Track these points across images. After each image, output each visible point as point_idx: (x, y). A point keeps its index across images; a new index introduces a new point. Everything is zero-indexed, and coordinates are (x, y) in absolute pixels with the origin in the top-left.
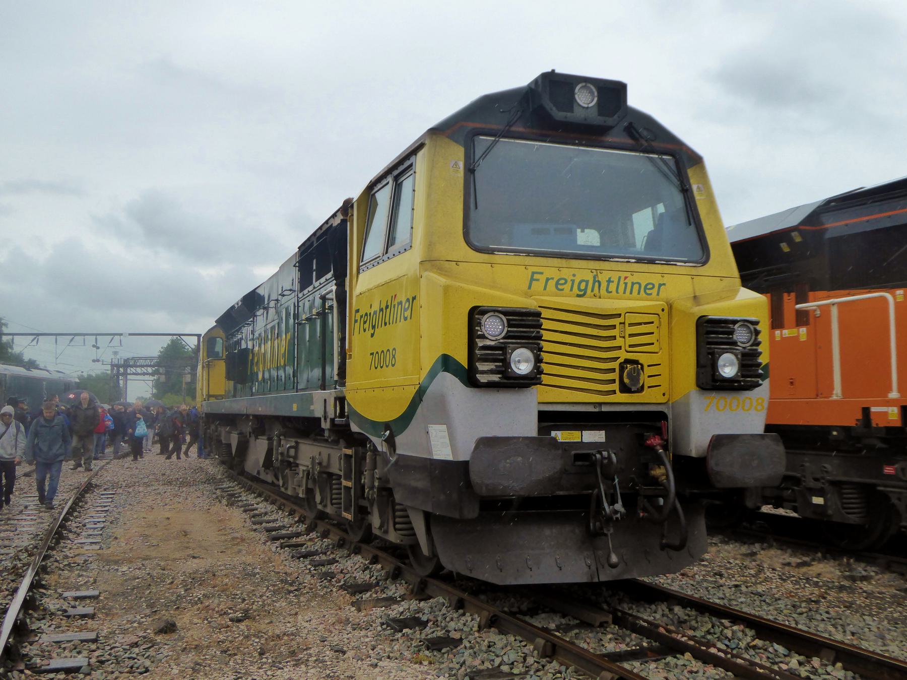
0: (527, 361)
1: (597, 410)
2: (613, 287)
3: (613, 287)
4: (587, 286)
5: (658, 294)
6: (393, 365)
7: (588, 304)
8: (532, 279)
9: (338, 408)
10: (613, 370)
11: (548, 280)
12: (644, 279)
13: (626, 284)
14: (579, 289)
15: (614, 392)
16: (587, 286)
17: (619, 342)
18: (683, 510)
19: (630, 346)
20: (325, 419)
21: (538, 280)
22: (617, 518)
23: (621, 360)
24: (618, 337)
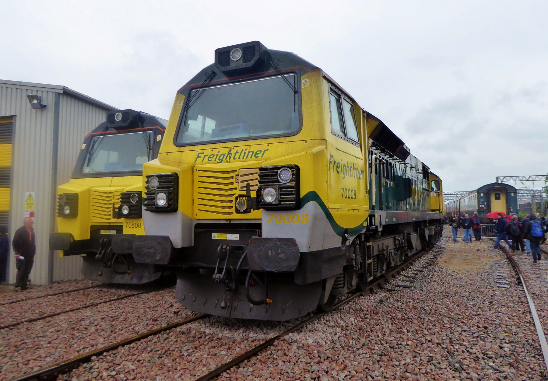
0: (164, 199)
1: (228, 222)
2: (237, 155)
3: (237, 155)
4: (223, 157)
5: (262, 156)
7: (224, 166)
8: (198, 157)
9: (373, 221)
10: (232, 201)
11: (205, 156)
12: (255, 149)
13: (245, 153)
14: (219, 159)
15: (232, 213)
16: (223, 157)
17: (235, 185)
18: (245, 280)
20: (380, 226)
23: (237, 195)
24: (234, 183)
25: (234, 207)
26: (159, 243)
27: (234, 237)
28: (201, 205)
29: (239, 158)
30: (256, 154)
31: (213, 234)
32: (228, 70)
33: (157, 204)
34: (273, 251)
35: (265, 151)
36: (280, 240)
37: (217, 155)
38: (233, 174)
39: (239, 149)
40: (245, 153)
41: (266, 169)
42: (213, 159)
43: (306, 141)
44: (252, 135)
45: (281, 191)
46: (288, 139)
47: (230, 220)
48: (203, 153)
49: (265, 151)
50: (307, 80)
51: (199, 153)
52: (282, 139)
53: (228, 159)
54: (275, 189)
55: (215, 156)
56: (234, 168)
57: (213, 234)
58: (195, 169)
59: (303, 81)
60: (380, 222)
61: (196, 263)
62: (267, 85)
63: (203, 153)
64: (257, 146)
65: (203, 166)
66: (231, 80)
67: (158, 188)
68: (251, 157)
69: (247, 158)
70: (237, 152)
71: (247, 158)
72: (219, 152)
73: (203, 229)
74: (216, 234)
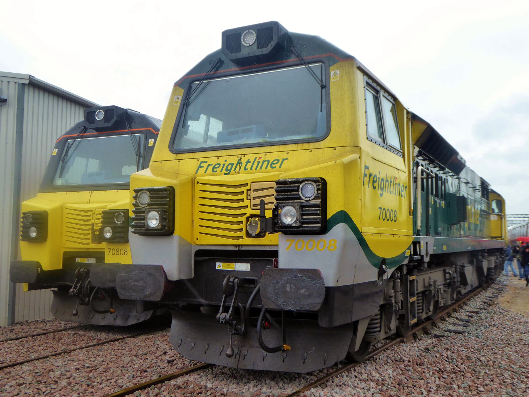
1: (237, 249)
2: (249, 166)
3: (249, 166)
5: (280, 167)
6: (395, 221)
7: (233, 178)
8: (200, 166)
10: (242, 222)
11: (209, 165)
12: (271, 157)
13: (259, 162)
14: (227, 170)
15: (242, 237)
17: (246, 203)
19: (254, 205)
20: (427, 255)
21: (203, 167)
22: (222, 322)
23: (248, 215)
24: (245, 199)
27: (244, 267)
29: (251, 169)
30: (272, 163)
31: (218, 264)
33: (148, 225)
36: (301, 271)
38: (244, 189)
39: (252, 158)
40: (259, 162)
41: (284, 183)
43: (335, 148)
45: (303, 211)
46: (312, 145)
47: (239, 246)
48: (206, 162)
49: (284, 160)
51: (202, 162)
52: (306, 146)
53: (237, 170)
54: (295, 208)
55: (222, 166)
56: (245, 180)
57: (218, 264)
58: (196, 182)
59: (332, 73)
62: (289, 77)
63: (206, 162)
64: (274, 153)
67: (149, 205)
68: (266, 168)
69: (261, 168)
70: (249, 161)
71: (261, 168)
72: (226, 161)
74: (221, 264)
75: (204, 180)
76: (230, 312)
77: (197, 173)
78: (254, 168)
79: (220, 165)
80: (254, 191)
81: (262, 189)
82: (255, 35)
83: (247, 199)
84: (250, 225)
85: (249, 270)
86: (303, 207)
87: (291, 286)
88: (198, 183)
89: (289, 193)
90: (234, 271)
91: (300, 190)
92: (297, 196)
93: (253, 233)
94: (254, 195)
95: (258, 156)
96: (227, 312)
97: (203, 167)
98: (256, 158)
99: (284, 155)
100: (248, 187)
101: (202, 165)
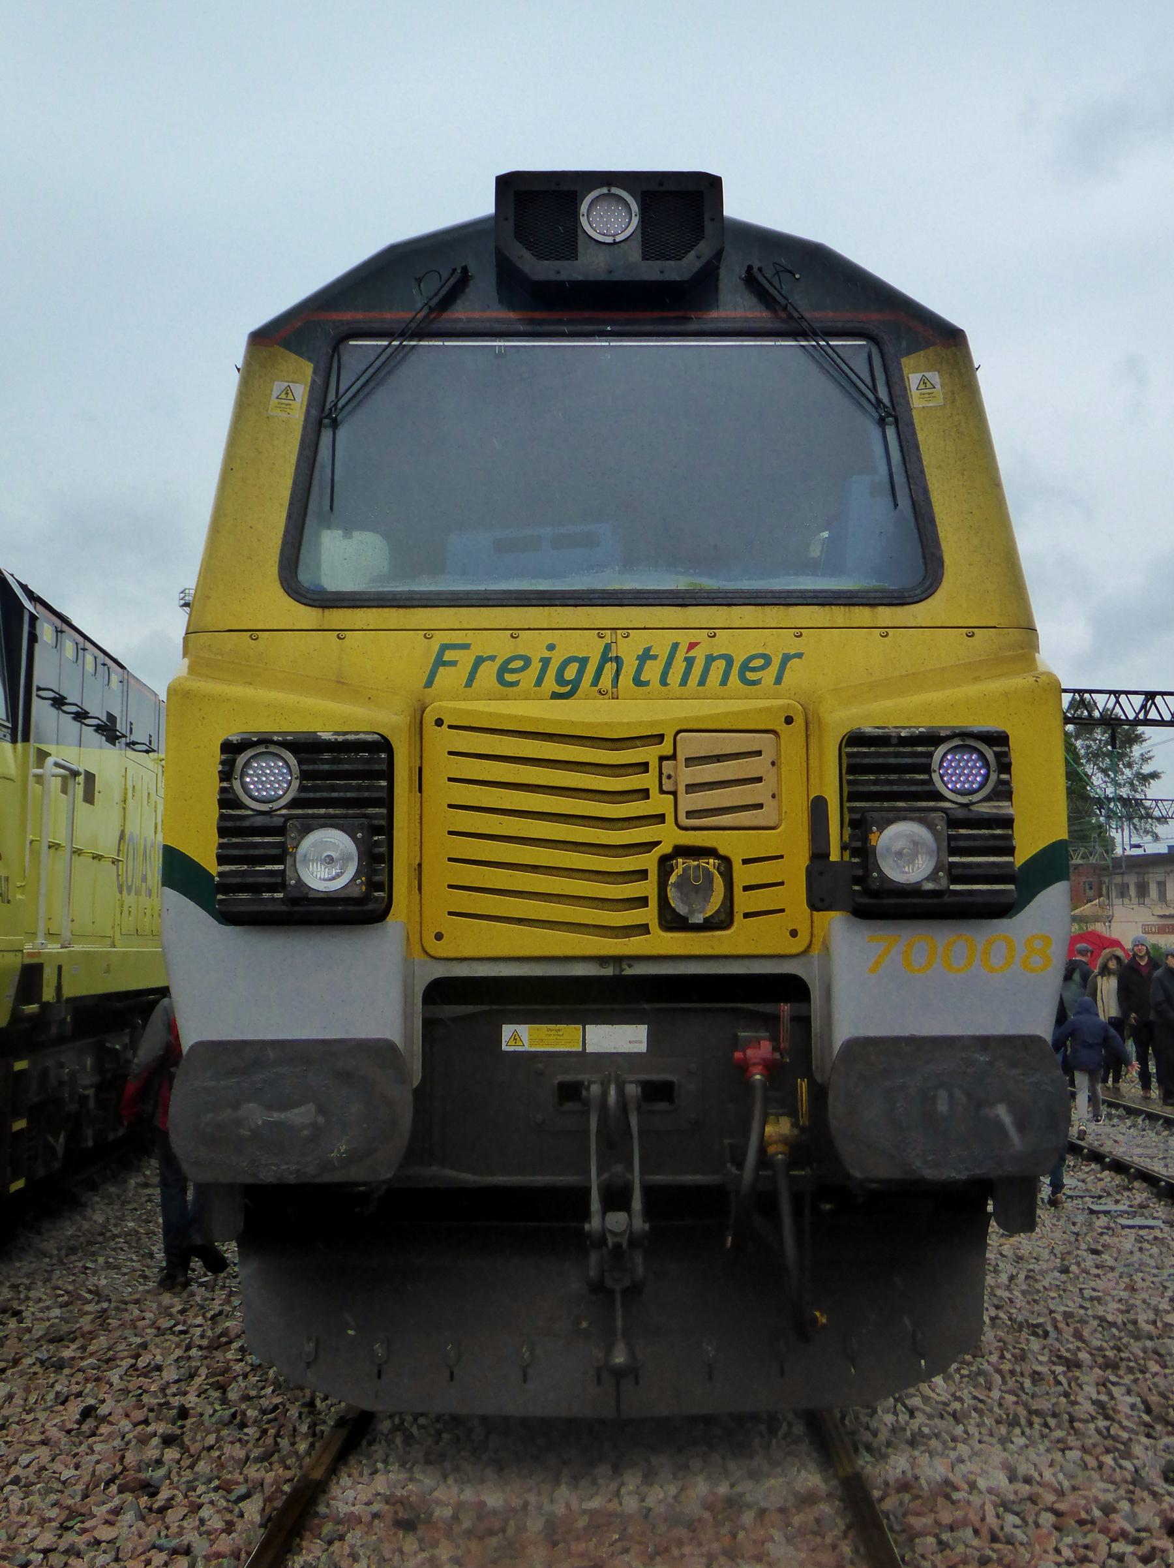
1: (609, 971)
2: (652, 672)
3: (652, 672)
4: (581, 673)
7: (586, 712)
8: (440, 662)
10: (643, 874)
11: (479, 661)
12: (741, 646)
13: (690, 662)
14: (560, 680)
15: (644, 929)
17: (659, 803)
19: (689, 814)
21: (454, 663)
23: (665, 848)
25: (653, 903)
26: (346, 1077)
27: (624, 1038)
28: (491, 895)
29: (664, 682)
30: (745, 667)
31: (507, 1030)
32: (564, 276)
33: (300, 883)
34: (958, 1093)
35: (786, 658)
36: (984, 1042)
37: (546, 662)
38: (649, 754)
39: (661, 644)
40: (690, 662)
41: (881, 740)
42: (528, 678)
43: (970, 631)
44: (709, 583)
45: (283, 845)
46: (885, 615)
47: (618, 960)
48: (466, 647)
49: (786, 658)
50: (934, 377)
51: (444, 648)
52: (862, 615)
53: (606, 681)
54: (931, 826)
55: (536, 666)
56: (653, 723)
57: (507, 1030)
58: (429, 718)
59: (913, 380)
60: (59, 988)
61: (435, 1169)
62: (728, 371)
63: (466, 647)
64: (744, 633)
65: (481, 706)
66: (531, 322)
67: (294, 803)
68: (724, 682)
69: (702, 682)
70: (646, 656)
71: (702, 682)
72: (551, 647)
73: (461, 1004)
74: (524, 1030)
75: (469, 713)
76: (637, 1204)
77: (429, 683)
78: (675, 677)
79: (527, 661)
80: (690, 761)
81: (719, 758)
82: (635, 207)
83: (662, 791)
84: (677, 885)
85: (643, 1048)
86: (953, 823)
87: (951, 1096)
88: (439, 722)
89: (893, 777)
90: (583, 1054)
91: (237, 775)
92: (927, 788)
93: (692, 912)
94: (688, 775)
95: (684, 638)
96: (626, 1206)
97: (454, 663)
98: (676, 646)
99: (786, 643)
100: (666, 748)
101: (449, 656)
